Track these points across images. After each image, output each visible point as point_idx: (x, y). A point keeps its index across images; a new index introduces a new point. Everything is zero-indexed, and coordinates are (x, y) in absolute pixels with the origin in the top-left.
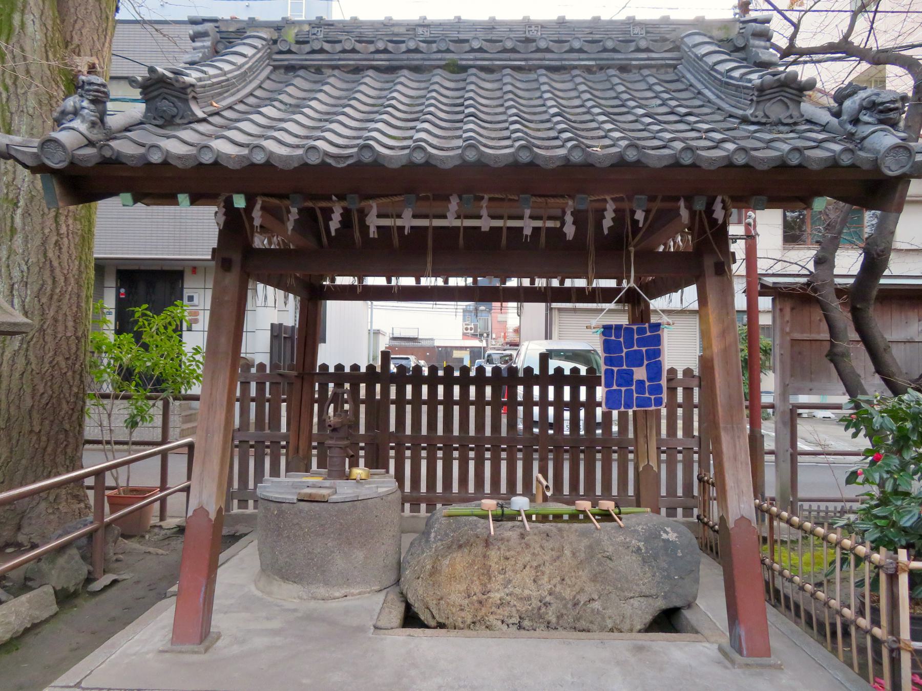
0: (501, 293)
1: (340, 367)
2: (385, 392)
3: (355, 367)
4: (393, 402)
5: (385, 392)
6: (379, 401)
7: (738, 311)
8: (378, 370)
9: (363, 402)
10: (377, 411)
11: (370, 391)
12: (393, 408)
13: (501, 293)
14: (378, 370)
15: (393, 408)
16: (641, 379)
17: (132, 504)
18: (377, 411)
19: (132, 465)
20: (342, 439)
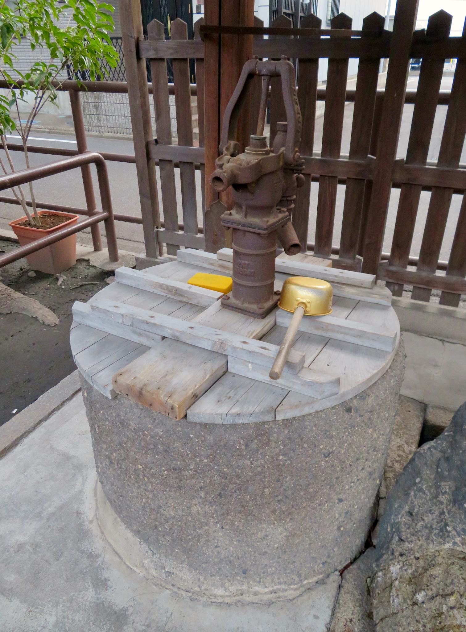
0: (328, 158)
1: (341, 21)
2: (397, 78)
3: (374, 21)
4: (410, 99)
5: (397, 78)
6: (381, 96)
7: (122, 90)
8: (389, 26)
9: (351, 97)
10: (377, 117)
11: (368, 75)
12: (408, 111)
13: (328, 158)
14: (389, 26)
15: (408, 111)
16: (382, 14)
17: (35, 239)
18: (377, 117)
19: (34, 182)
20: (265, 210)
